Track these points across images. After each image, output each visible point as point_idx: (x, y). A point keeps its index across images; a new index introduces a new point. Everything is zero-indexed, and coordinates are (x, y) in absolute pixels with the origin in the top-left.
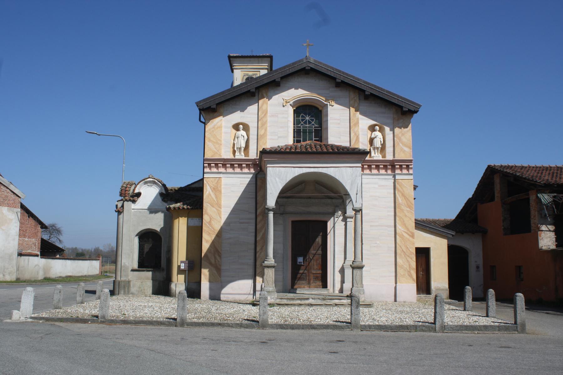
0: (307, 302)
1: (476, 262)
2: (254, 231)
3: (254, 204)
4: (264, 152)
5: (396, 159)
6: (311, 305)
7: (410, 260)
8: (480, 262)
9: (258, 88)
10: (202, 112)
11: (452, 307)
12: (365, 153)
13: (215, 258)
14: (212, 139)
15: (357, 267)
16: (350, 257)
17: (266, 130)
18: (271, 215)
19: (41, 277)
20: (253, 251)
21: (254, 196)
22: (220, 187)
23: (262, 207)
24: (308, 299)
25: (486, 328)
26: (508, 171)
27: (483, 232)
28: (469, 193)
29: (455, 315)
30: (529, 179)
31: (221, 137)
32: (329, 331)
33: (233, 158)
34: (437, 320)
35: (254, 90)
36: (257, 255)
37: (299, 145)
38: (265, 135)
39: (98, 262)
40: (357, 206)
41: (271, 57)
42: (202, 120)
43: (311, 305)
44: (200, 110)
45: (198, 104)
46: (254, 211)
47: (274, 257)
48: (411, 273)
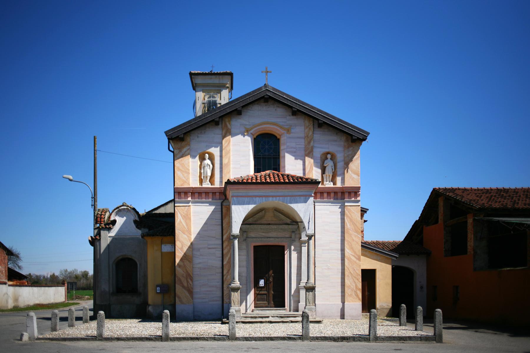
0: (267, 320)
1: (420, 282)
2: (221, 255)
3: (220, 231)
4: (229, 183)
5: (345, 186)
6: (271, 322)
7: (356, 281)
8: (424, 282)
9: (222, 117)
10: (171, 141)
11: (387, 322)
12: (316, 183)
13: (188, 282)
14: (181, 168)
15: (311, 289)
16: (304, 279)
17: (229, 159)
18: (236, 242)
19: (11, 305)
20: (221, 275)
21: (220, 223)
22: (190, 215)
23: (228, 233)
24: (268, 317)
25: (410, 338)
26: (451, 194)
27: (428, 254)
28: (416, 216)
29: (387, 328)
30: (466, 204)
31: (189, 166)
32: (286, 341)
33: (200, 186)
34: (371, 332)
35: (217, 120)
36: (224, 278)
37: (259, 175)
38: (228, 164)
39: (64, 288)
40: (310, 232)
41: (231, 74)
42: (171, 149)
43: (271, 322)
44: (169, 139)
45: (166, 133)
46: (221, 237)
47: (239, 279)
48: (357, 293)
